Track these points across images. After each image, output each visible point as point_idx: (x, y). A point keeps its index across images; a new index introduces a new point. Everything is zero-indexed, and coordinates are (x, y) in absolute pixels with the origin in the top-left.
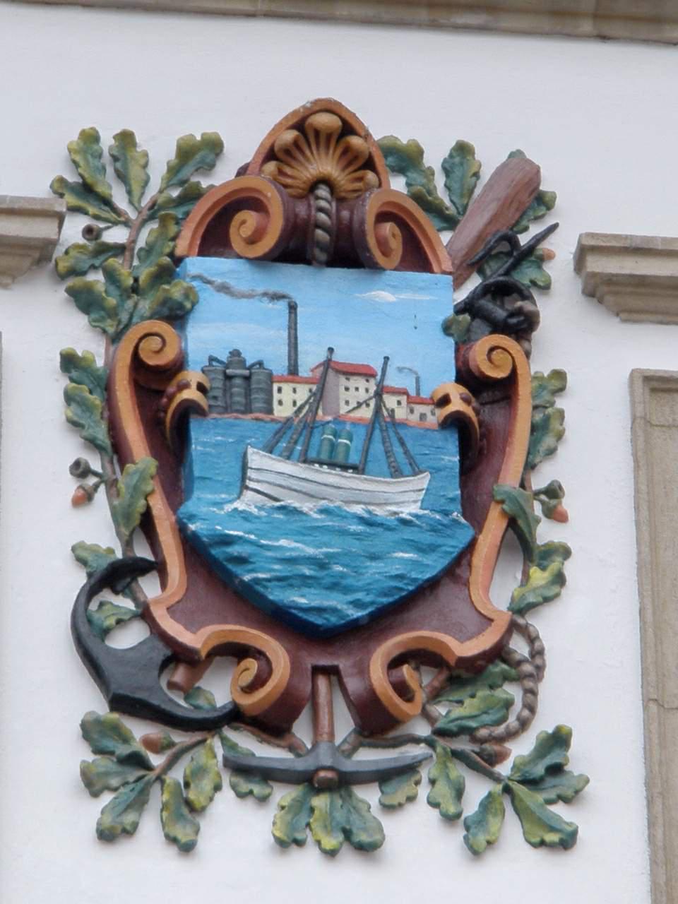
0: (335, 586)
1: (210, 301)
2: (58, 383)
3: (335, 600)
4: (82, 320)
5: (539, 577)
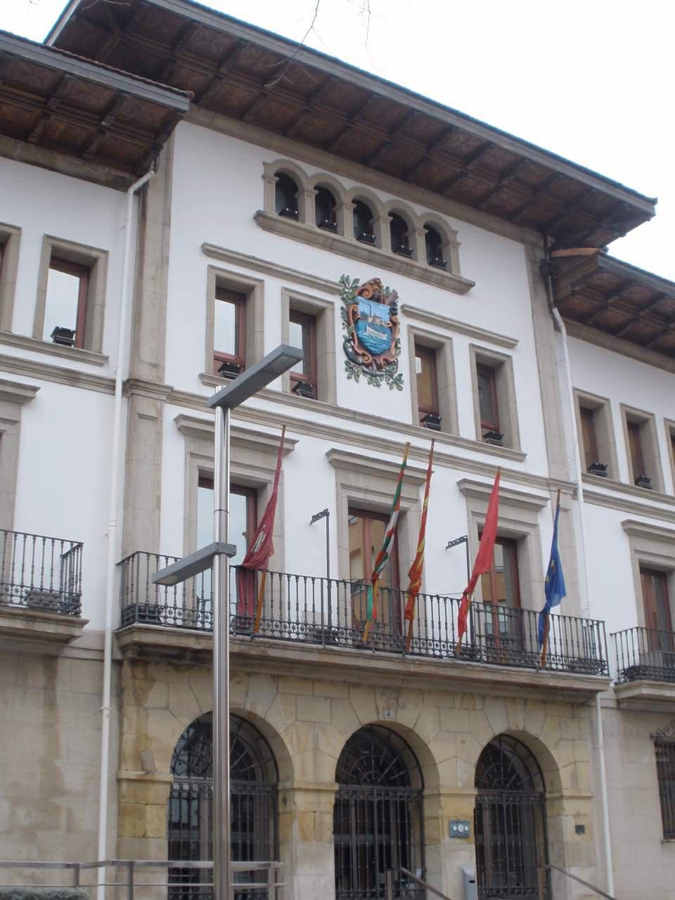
0: (376, 348)
1: (360, 303)
2: (340, 311)
3: (376, 350)
4: (342, 302)
5: (398, 351)
